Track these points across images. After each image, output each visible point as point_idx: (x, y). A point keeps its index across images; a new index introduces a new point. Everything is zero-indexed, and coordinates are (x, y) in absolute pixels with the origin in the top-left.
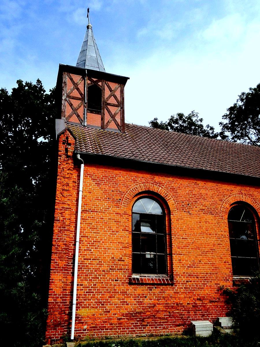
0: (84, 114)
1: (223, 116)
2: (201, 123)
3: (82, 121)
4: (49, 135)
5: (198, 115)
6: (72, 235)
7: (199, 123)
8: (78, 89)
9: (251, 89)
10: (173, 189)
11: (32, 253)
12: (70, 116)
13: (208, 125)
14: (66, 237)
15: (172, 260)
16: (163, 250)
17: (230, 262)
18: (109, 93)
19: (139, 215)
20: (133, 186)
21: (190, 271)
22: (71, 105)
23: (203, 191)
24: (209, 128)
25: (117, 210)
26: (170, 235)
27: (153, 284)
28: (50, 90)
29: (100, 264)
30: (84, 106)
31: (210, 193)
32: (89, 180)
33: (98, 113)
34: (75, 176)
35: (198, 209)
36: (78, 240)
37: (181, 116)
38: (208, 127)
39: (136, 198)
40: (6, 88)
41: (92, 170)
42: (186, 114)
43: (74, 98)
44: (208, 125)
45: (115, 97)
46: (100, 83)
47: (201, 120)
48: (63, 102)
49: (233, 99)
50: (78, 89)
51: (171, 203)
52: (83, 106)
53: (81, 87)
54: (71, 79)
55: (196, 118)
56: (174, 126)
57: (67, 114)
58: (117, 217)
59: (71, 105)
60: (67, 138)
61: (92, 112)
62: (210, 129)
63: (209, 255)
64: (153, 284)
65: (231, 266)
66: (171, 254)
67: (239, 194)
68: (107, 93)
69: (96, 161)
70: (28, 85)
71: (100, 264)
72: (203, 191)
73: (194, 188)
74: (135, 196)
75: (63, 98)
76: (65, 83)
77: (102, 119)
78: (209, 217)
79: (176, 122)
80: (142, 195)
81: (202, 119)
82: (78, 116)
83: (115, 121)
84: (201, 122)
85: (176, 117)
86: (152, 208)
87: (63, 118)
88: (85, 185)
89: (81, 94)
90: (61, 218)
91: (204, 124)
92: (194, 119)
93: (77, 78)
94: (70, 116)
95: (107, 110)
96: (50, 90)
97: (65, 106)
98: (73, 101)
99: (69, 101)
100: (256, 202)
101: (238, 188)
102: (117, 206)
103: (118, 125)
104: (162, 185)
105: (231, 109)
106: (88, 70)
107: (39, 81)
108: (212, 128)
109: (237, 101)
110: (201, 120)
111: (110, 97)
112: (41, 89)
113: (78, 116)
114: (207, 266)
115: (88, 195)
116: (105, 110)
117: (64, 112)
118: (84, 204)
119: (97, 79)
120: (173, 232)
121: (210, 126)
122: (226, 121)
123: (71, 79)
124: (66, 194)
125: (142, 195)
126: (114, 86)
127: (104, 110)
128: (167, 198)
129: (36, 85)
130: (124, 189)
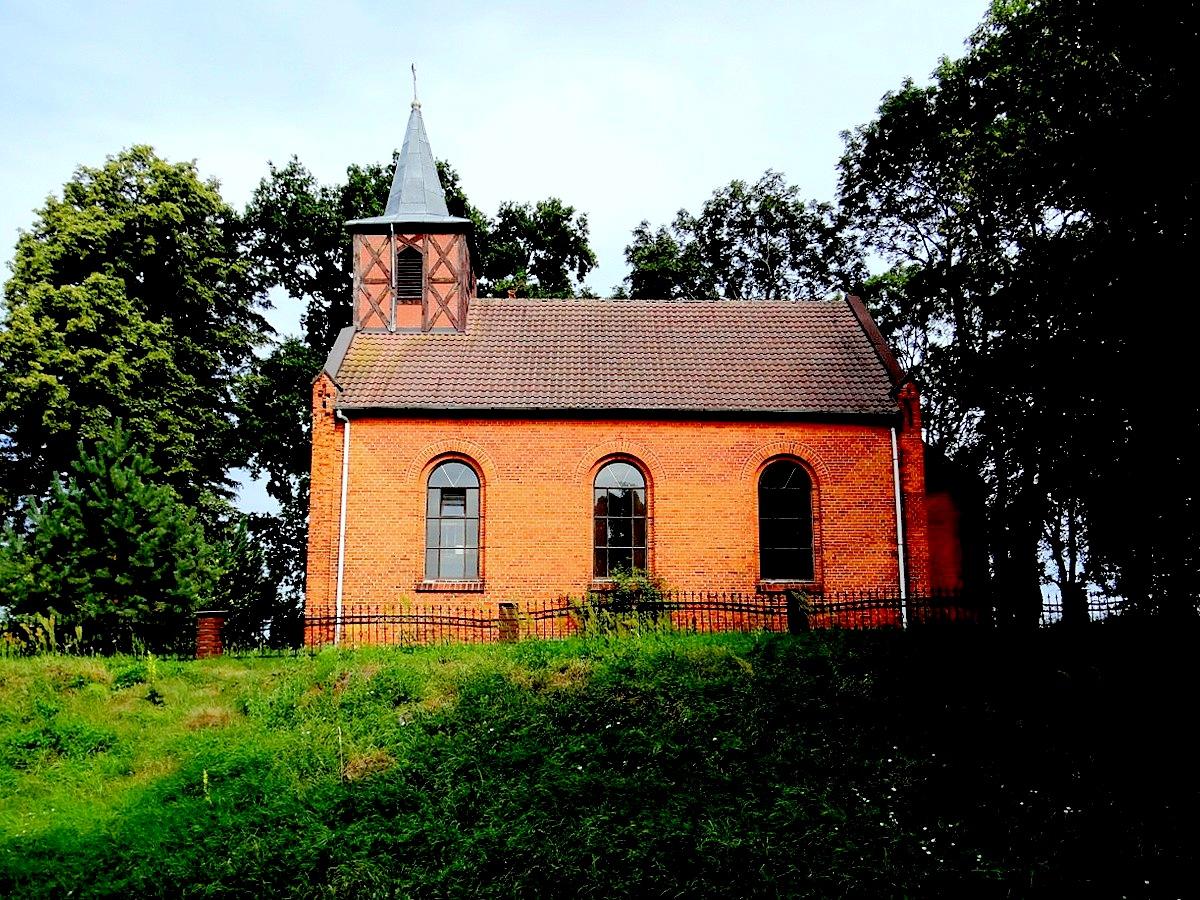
4: (1061, 39)
6: (335, 528)
8: (380, 263)
11: (855, 793)
12: (367, 317)
14: (324, 532)
18: (448, 257)
21: (514, 572)
22: (368, 296)
23: (546, 443)
25: (401, 487)
27: (452, 592)
29: (375, 564)
32: (360, 446)
33: (417, 301)
34: (338, 441)
36: (342, 533)
39: (599, 465)
40: (338, 183)
41: (355, 426)
43: (373, 282)
45: (448, 265)
46: (419, 243)
51: (487, 467)
52: (389, 294)
54: (367, 246)
58: (402, 498)
59: (368, 296)
61: (404, 302)
64: (452, 592)
69: (357, 415)
71: (375, 564)
72: (546, 443)
86: (620, 477)
88: (353, 455)
89: (385, 271)
90: (319, 505)
98: (371, 288)
100: (649, 452)
102: (401, 479)
103: (452, 320)
104: (471, 439)
115: (359, 468)
116: (430, 293)
118: (353, 481)
119: (414, 235)
123: (367, 246)
124: (324, 470)
125: (602, 463)
127: (426, 293)
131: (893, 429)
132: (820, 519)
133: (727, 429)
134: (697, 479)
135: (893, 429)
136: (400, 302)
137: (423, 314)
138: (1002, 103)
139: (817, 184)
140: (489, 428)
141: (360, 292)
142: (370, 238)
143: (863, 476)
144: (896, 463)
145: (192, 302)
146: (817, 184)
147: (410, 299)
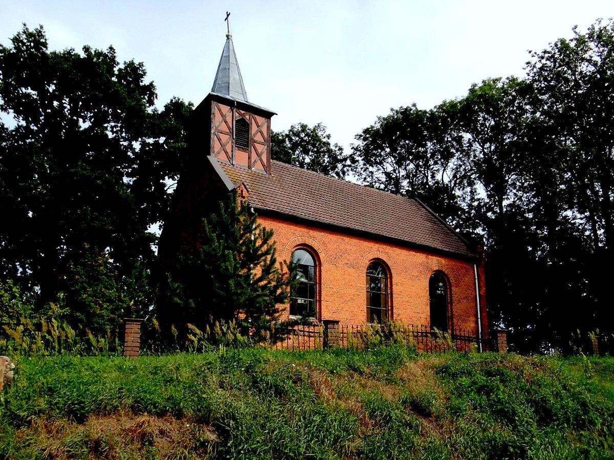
0: (232, 151)
1: (356, 136)
2: (328, 141)
3: (230, 158)
5: (326, 130)
7: (325, 140)
8: (226, 122)
9: (392, 110)
10: (324, 243)
12: (219, 153)
13: (337, 144)
15: (321, 306)
16: (312, 296)
17: (366, 311)
19: (369, 277)
20: (292, 239)
22: (219, 140)
23: (348, 247)
24: (337, 148)
26: (320, 284)
28: (125, 62)
30: (232, 142)
31: (354, 249)
33: (244, 150)
35: (343, 263)
37: (304, 127)
38: (336, 147)
39: (296, 248)
42: (311, 126)
44: (337, 144)
47: (329, 137)
48: (212, 136)
49: (371, 121)
50: (226, 122)
51: (322, 256)
52: (230, 142)
53: (229, 119)
54: (220, 110)
55: (323, 133)
56: (294, 139)
57: (216, 150)
59: (219, 140)
60: (242, 191)
62: (338, 150)
63: (350, 304)
65: (366, 314)
66: (320, 301)
67: (377, 251)
68: (254, 129)
70: (99, 54)
72: (348, 247)
73: (341, 243)
74: (296, 246)
75: (212, 132)
76: (213, 114)
77: (249, 158)
78: (351, 271)
79: (297, 134)
80: (300, 247)
81: (329, 135)
82: (226, 153)
83: (261, 160)
84: (328, 139)
85: (298, 128)
86: (306, 258)
87: (211, 154)
89: (229, 128)
91: (332, 142)
92: (320, 134)
93: (225, 109)
94: (219, 153)
95: (254, 148)
96: (125, 62)
97: (214, 141)
99: (218, 135)
101: (377, 246)
103: (263, 165)
104: (316, 239)
105: (366, 131)
106: (237, 102)
107: (111, 48)
108: (340, 149)
109: (375, 124)
110: (329, 137)
111: (256, 133)
112: (113, 59)
113: (226, 153)
114: (347, 313)
117: (213, 147)
120: (322, 282)
121: (338, 145)
122: (360, 143)
123: (220, 110)
125: (300, 247)
126: (261, 120)
128: (319, 252)
129: (107, 53)
130: (285, 241)
131: (475, 265)
132: (451, 303)
133: (419, 254)
134: (409, 277)
135: (475, 265)
136: (236, 148)
137: (249, 158)
138: (172, 114)
139: (344, 137)
140: (323, 234)
141: (215, 136)
142: (222, 106)
143: (465, 285)
144: (477, 280)
145: (94, 110)
146: (344, 137)
147: (242, 148)
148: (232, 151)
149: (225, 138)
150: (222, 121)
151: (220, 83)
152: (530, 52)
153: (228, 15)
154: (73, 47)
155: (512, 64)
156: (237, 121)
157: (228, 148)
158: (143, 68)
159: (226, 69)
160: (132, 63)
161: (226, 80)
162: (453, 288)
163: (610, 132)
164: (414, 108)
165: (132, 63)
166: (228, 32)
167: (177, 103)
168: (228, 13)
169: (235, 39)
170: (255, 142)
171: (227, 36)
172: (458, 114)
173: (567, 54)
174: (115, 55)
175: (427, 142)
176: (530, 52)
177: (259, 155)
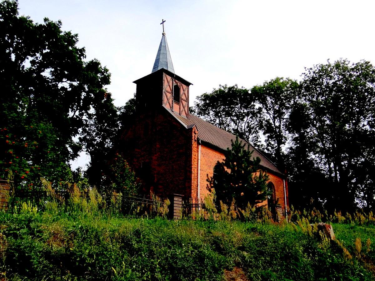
0: (172, 104)
8: (169, 86)
50: (169, 86)
54: (167, 79)
57: (165, 102)
60: (195, 130)
75: (163, 91)
82: (169, 104)
83: (185, 110)
93: (169, 78)
123: (167, 79)
126: (185, 86)
142: (168, 76)
148: (172, 104)
149: (169, 95)
150: (167, 84)
151: (161, 61)
152: (305, 68)
153: (163, 22)
154: (29, 16)
155: (296, 72)
156: (174, 86)
157: (171, 101)
158: (77, 37)
159: (164, 54)
160: (70, 33)
161: (165, 60)
162: (276, 192)
163: (2, 71)
164: (236, 87)
165: (70, 33)
166: (163, 31)
167: (96, 63)
168: (164, 21)
169: (166, 35)
170: (182, 99)
171: (163, 34)
172: (258, 94)
173: (324, 71)
174: (61, 26)
175: (59, 88)
176: (305, 68)
177: (184, 107)
